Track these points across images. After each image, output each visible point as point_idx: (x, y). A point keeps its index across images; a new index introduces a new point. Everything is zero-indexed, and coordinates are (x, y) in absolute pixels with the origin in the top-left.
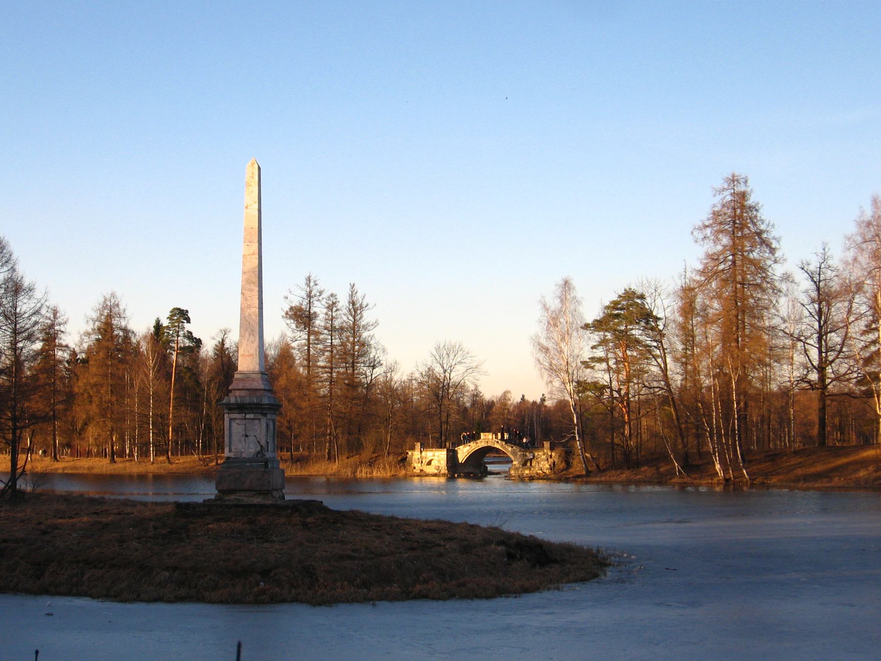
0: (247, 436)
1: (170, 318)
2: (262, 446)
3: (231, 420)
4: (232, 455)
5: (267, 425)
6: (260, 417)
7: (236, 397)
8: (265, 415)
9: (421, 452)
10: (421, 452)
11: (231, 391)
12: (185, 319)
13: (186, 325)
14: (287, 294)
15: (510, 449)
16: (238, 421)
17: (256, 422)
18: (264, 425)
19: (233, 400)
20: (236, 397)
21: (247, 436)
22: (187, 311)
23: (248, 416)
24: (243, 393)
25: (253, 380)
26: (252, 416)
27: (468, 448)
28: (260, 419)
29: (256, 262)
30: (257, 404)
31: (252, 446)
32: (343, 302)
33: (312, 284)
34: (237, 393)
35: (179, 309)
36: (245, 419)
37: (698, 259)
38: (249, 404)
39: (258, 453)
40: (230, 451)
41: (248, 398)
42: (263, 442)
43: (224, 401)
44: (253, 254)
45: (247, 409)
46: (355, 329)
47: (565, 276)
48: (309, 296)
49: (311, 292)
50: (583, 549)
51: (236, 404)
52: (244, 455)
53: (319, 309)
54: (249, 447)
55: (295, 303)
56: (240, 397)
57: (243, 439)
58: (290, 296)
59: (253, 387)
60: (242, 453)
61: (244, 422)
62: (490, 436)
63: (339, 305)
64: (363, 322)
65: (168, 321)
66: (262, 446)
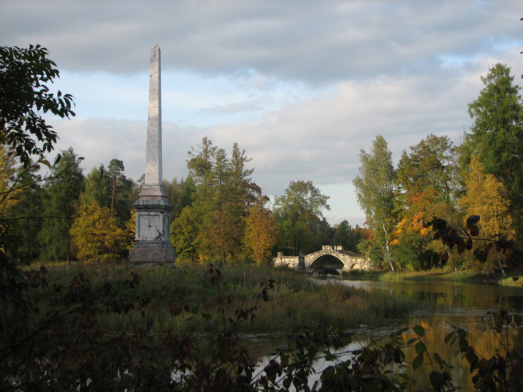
0: (150, 226)
1: (110, 167)
2: (160, 234)
3: (140, 215)
5: (164, 220)
6: (159, 214)
7: (143, 201)
8: (162, 212)
9: (281, 259)
10: (281, 259)
11: (140, 197)
12: (121, 167)
13: (121, 172)
14: (191, 150)
15: (342, 257)
16: (144, 217)
17: (157, 217)
18: (161, 219)
19: (141, 203)
20: (143, 201)
21: (150, 226)
22: (122, 162)
23: (151, 213)
24: (148, 198)
26: (153, 213)
27: (313, 256)
28: (159, 215)
29: (157, 112)
30: (156, 205)
31: (153, 233)
32: (229, 156)
33: (208, 144)
34: (144, 198)
35: (115, 160)
36: (149, 215)
37: (470, 128)
39: (157, 238)
40: (139, 236)
42: (161, 231)
43: (136, 204)
44: (156, 107)
45: (150, 208)
46: (238, 174)
48: (206, 151)
49: (207, 149)
51: (143, 205)
52: (148, 239)
53: (213, 160)
54: (151, 234)
56: (146, 201)
57: (148, 228)
58: (193, 152)
59: (155, 194)
61: (148, 217)
62: (329, 248)
63: (227, 157)
64: (244, 169)
65: (109, 169)
66: (160, 234)
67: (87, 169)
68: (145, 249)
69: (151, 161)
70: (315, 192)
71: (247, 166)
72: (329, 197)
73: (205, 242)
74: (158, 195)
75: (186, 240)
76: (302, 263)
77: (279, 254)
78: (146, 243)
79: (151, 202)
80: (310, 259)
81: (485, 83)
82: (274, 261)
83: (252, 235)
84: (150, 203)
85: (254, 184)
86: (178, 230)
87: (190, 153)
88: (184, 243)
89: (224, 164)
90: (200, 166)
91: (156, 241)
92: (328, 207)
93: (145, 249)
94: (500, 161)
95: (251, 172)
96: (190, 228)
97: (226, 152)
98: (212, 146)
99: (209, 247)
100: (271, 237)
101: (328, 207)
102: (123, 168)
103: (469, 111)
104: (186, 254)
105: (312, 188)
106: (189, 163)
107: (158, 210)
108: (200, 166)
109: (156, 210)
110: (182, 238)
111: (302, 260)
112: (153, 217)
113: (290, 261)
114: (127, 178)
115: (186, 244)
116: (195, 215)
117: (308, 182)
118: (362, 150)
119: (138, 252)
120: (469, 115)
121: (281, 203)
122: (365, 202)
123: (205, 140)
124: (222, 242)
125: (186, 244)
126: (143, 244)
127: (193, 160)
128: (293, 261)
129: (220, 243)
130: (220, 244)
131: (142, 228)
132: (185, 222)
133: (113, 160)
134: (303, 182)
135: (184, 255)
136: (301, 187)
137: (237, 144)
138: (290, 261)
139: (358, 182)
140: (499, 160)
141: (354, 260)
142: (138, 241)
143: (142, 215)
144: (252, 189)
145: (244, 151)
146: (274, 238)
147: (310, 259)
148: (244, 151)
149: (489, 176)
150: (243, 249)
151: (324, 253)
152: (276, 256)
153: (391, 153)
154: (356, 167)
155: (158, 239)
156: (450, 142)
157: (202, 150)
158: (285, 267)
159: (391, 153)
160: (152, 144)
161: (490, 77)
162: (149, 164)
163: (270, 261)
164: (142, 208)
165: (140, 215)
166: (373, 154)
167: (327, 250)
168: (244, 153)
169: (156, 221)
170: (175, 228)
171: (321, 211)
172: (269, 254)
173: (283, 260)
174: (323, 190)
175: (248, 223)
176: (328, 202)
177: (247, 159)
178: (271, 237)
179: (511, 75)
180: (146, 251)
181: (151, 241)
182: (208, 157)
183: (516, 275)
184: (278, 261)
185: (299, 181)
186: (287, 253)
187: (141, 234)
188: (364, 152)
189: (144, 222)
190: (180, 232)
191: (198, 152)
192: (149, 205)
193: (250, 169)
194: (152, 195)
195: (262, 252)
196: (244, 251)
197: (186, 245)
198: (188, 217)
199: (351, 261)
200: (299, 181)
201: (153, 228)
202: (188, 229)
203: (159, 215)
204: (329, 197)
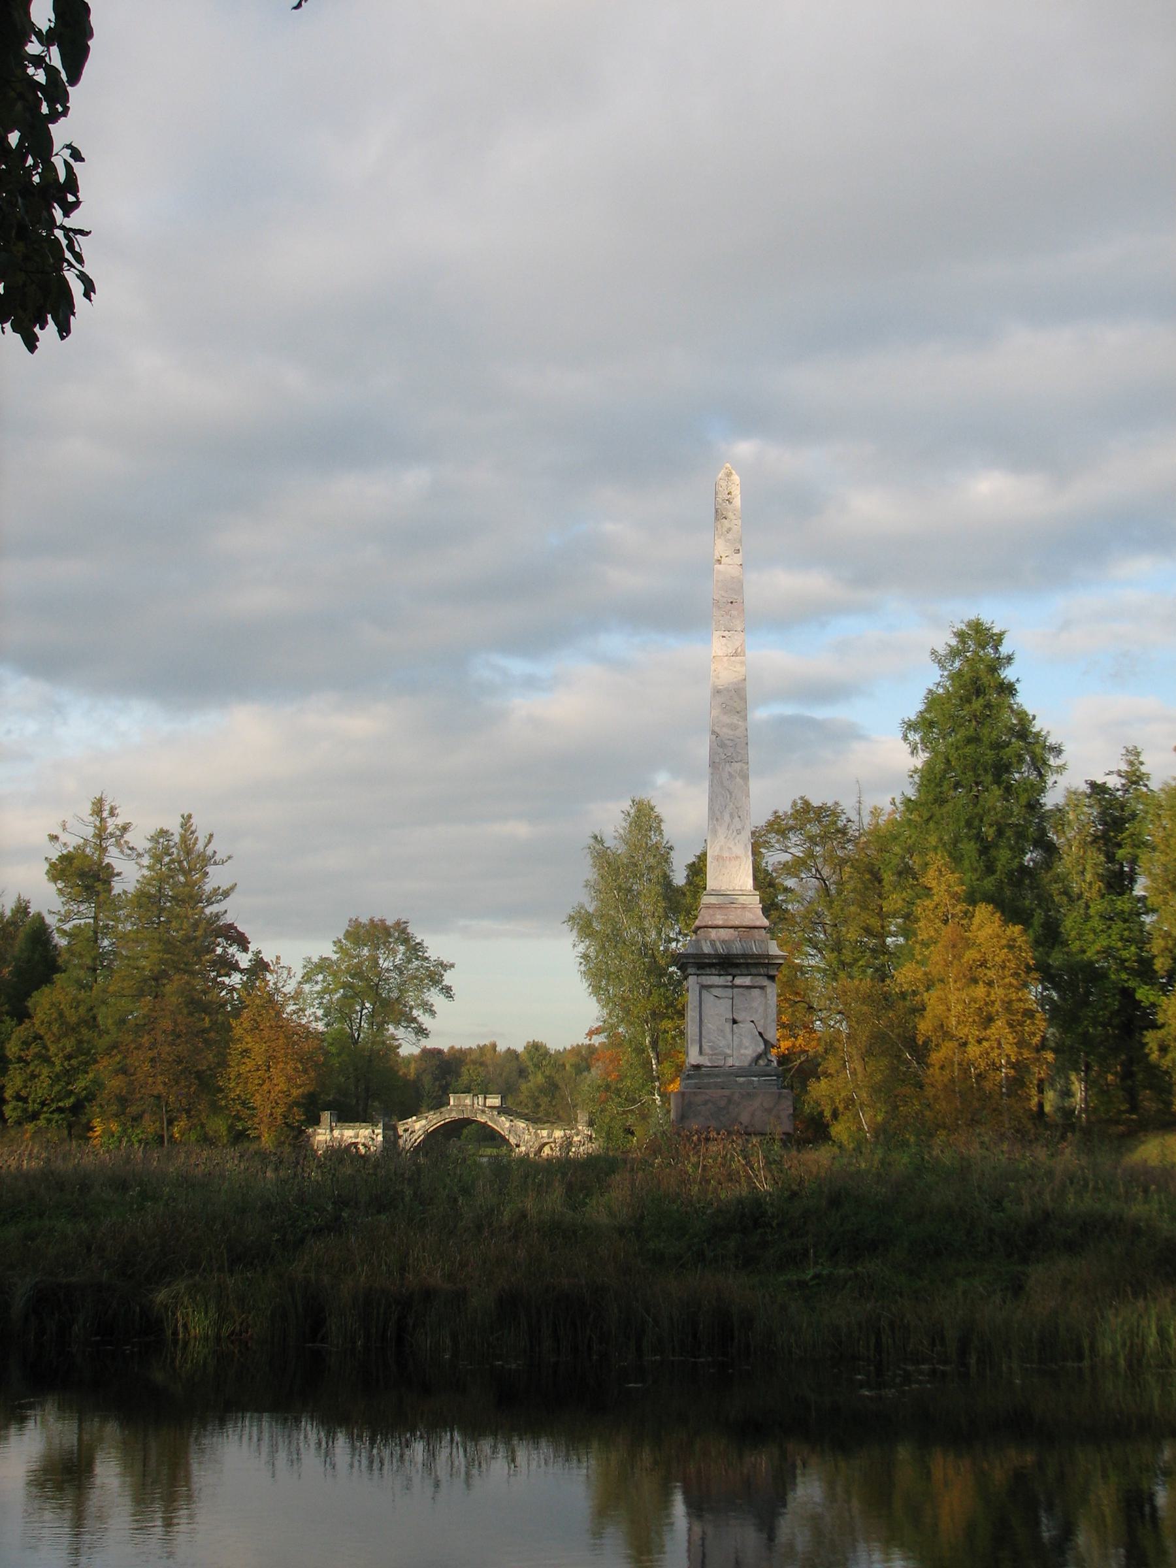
0: (735, 1022)
4: (704, 1061)
6: (765, 982)
7: (713, 943)
9: (332, 1130)
10: (332, 1130)
14: (57, 831)
15: (508, 1124)
16: (716, 992)
17: (756, 992)
18: (773, 1000)
21: (735, 1022)
23: (739, 981)
24: (724, 934)
25: (744, 907)
26: (747, 981)
27: (424, 1122)
28: (762, 988)
33: (105, 814)
34: (713, 934)
36: (733, 987)
38: (744, 956)
39: (759, 1057)
40: (701, 1052)
41: (738, 945)
45: (737, 965)
47: (774, 809)
50: (61, 1408)
52: (730, 1062)
54: (740, 1046)
55: (71, 841)
56: (723, 942)
57: (728, 1026)
58: (64, 837)
60: (726, 1056)
68: (727, 1092)
69: (727, 817)
70: (415, 950)
71: (216, 878)
72: (452, 966)
73: (115, 1084)
74: (758, 924)
75: (56, 1079)
76: (391, 1138)
77: (326, 1116)
80: (417, 1127)
81: (943, 667)
82: (309, 1137)
83: (250, 1064)
84: (737, 948)
85: (231, 926)
86: (34, 1049)
87: (54, 838)
88: (52, 1085)
90: (82, 875)
91: (755, 1068)
92: (447, 991)
93: (727, 1092)
94: (993, 872)
95: (226, 894)
96: (69, 1044)
98: (120, 821)
99: (123, 1101)
100: (305, 1071)
101: (447, 991)
103: (905, 738)
104: (56, 1116)
105: (406, 939)
106: (53, 865)
107: (762, 971)
108: (82, 875)
109: (754, 971)
110: (45, 1072)
111: (391, 1133)
113: (357, 1136)
115: (57, 1088)
116: (82, 1010)
117: (398, 923)
118: (595, 837)
119: (705, 1103)
120: (906, 748)
121: (320, 977)
122: (600, 976)
123: (98, 807)
124: (165, 1084)
125: (57, 1088)
126: (717, 1076)
127: (67, 859)
128: (363, 1136)
129: (161, 1087)
130: (160, 1089)
131: (710, 1025)
132: (55, 1028)
134: (383, 921)
135: (49, 1121)
136: (374, 934)
137: (190, 816)
138: (357, 1136)
139: (583, 924)
140: (990, 869)
141: (545, 1133)
142: (697, 1067)
144: (227, 938)
145: (211, 835)
146: (313, 1074)
147: (417, 1127)
148: (211, 835)
149: (983, 911)
150: (223, 1103)
151: (455, 1115)
152: (316, 1122)
153: (671, 848)
154: (578, 885)
155: (761, 1062)
156: (843, 817)
157: (89, 832)
158: (342, 1153)
159: (671, 848)
160: (728, 768)
161: (954, 653)
162: (722, 832)
163: (297, 1135)
164: (711, 965)
165: (703, 987)
166: (622, 849)
167: (460, 1105)
168: (209, 842)
169: (755, 1005)
170: (26, 1044)
171: (431, 1001)
172: (298, 1115)
173: (336, 1133)
174: (436, 947)
175: (238, 1032)
176: (448, 978)
177: (217, 858)
178: (305, 1071)
179: (1004, 650)
180: (730, 1100)
181: (740, 1068)
182: (105, 850)
184: (324, 1136)
185: (372, 921)
186: (347, 1116)
187: (705, 1046)
188: (601, 842)
189: (716, 1009)
190: (38, 1056)
191: (78, 833)
192: (737, 956)
193: (224, 887)
194: (737, 923)
195: (279, 1111)
196: (221, 1108)
197: (59, 1092)
198: (61, 1015)
199: (536, 1135)
200: (372, 921)
201: (745, 1027)
202: (64, 1048)
203: (762, 988)
204: (452, 966)
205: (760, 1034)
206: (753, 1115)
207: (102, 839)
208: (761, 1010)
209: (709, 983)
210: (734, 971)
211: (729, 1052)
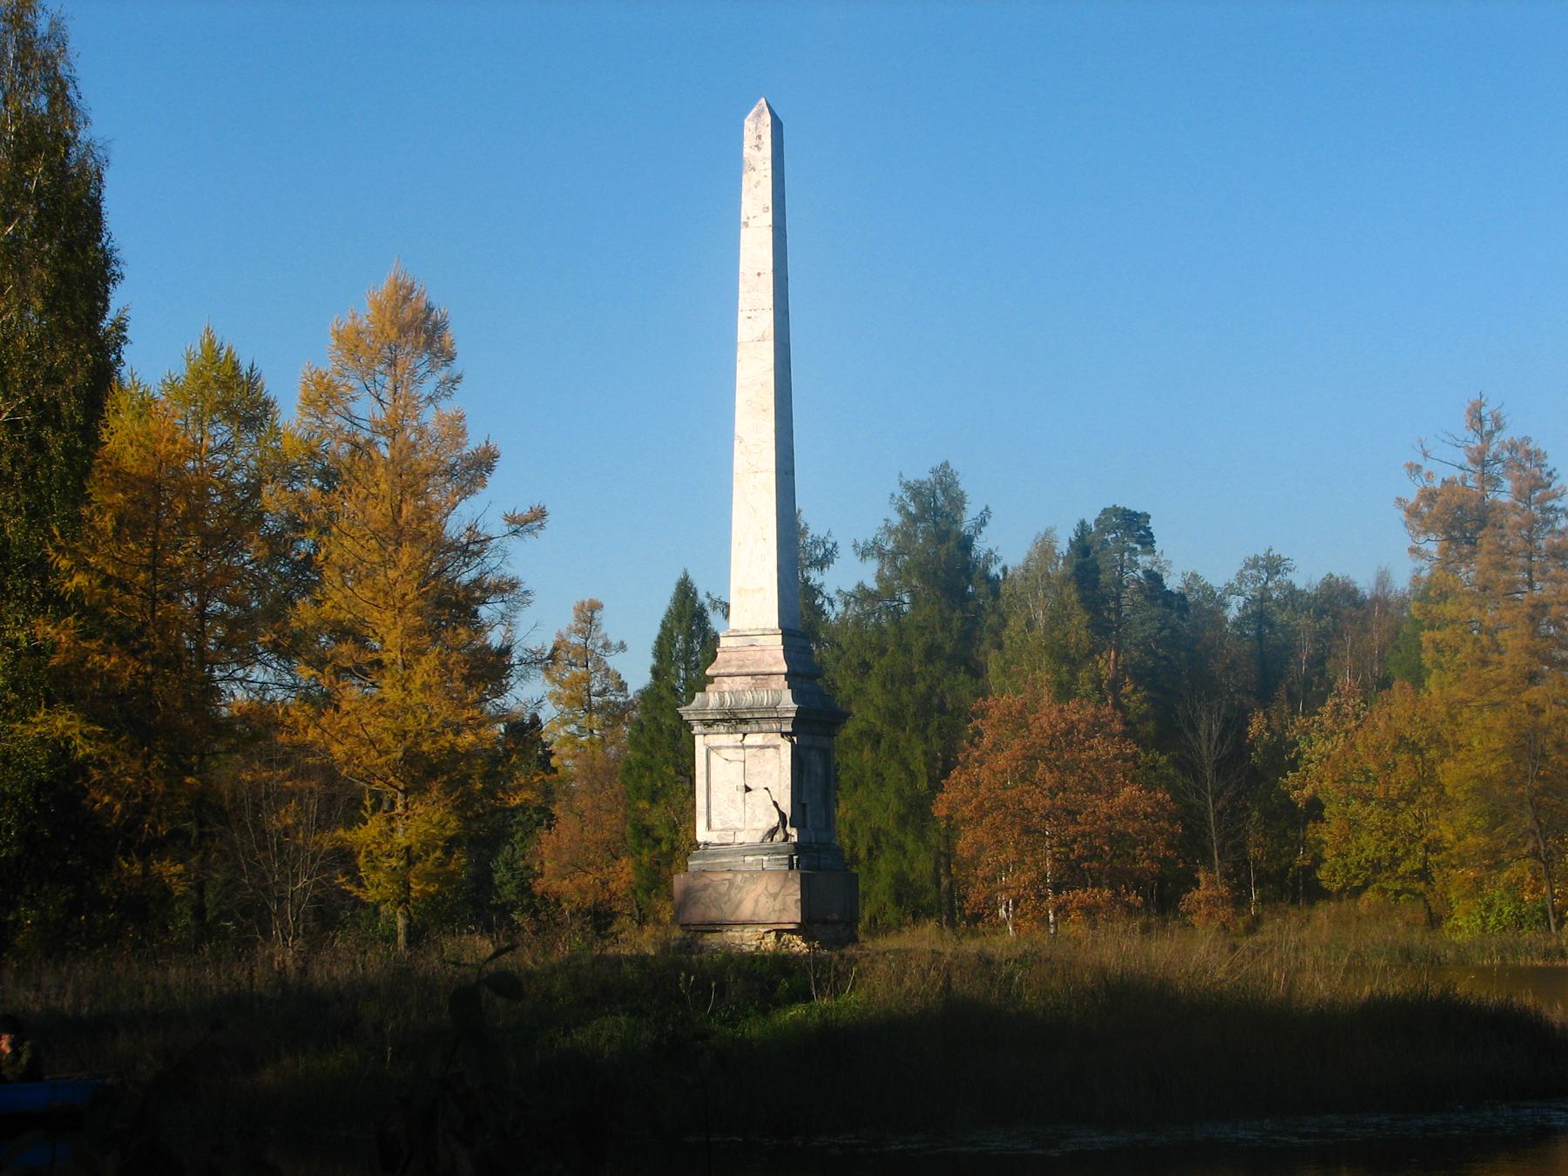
0: (748, 789)
2: (782, 815)
14: (1418, 459)
16: (727, 753)
20: (721, 694)
23: (749, 740)
28: (776, 747)
31: (760, 813)
35: (1115, 511)
36: (743, 747)
39: (772, 832)
42: (786, 806)
44: (762, 339)
45: (745, 721)
48: (1480, 460)
52: (741, 838)
57: (741, 793)
58: (1427, 466)
61: (740, 754)
67: (1006, 545)
74: (775, 670)
78: (736, 853)
79: (749, 696)
84: (748, 698)
87: (1414, 469)
89: (1545, 510)
97: (1550, 463)
102: (1147, 541)
109: (765, 727)
112: (759, 753)
114: (1173, 583)
123: (1476, 416)
127: (1429, 496)
133: (1105, 511)
143: (719, 748)
157: (1462, 457)
169: (769, 768)
181: (753, 844)
183: (818, 962)
191: (1448, 464)
201: (758, 796)
203: (776, 747)
205: (775, 804)
206: (757, 902)
207: (1483, 464)
208: (775, 775)
209: (717, 744)
210: (744, 728)
211: (740, 825)
